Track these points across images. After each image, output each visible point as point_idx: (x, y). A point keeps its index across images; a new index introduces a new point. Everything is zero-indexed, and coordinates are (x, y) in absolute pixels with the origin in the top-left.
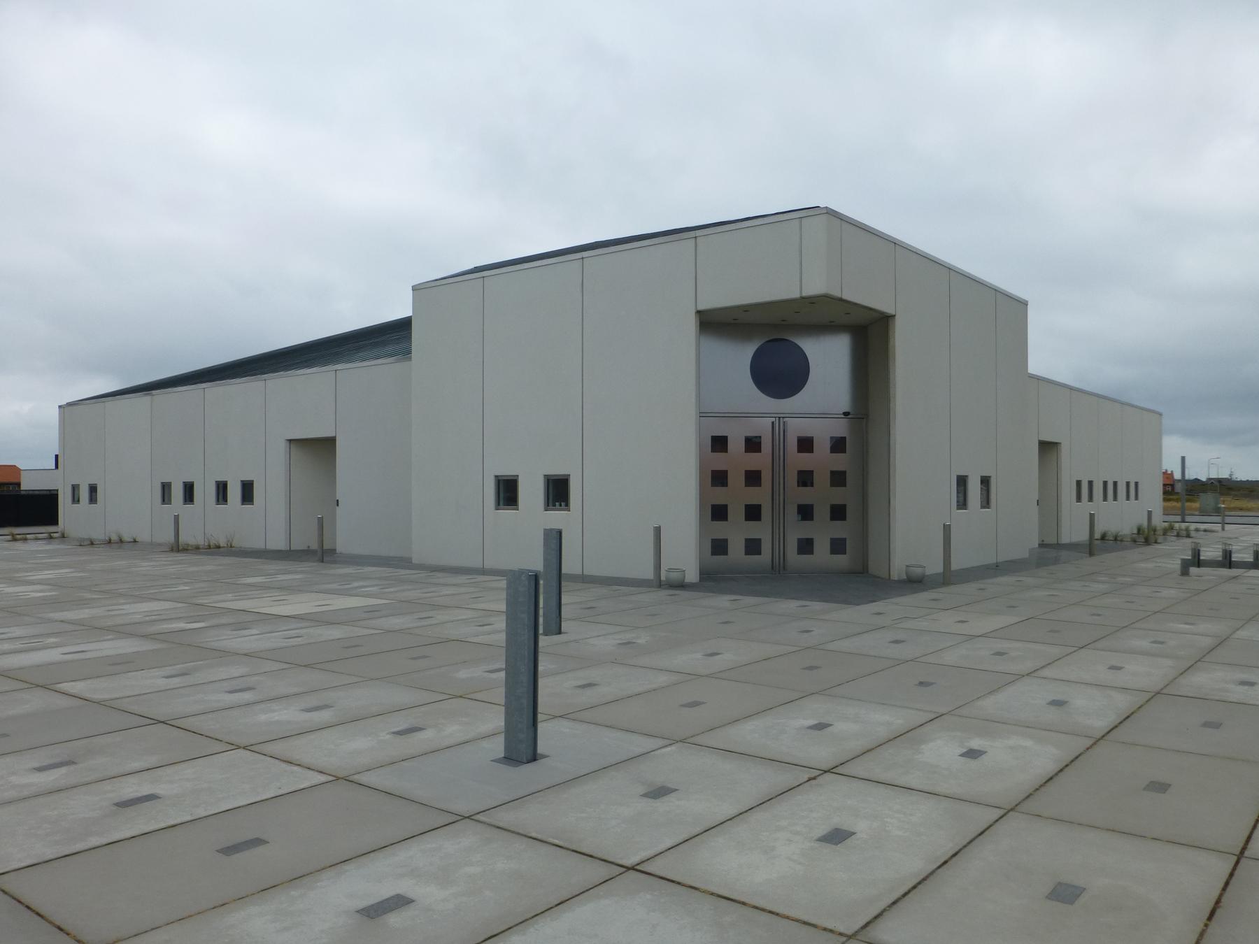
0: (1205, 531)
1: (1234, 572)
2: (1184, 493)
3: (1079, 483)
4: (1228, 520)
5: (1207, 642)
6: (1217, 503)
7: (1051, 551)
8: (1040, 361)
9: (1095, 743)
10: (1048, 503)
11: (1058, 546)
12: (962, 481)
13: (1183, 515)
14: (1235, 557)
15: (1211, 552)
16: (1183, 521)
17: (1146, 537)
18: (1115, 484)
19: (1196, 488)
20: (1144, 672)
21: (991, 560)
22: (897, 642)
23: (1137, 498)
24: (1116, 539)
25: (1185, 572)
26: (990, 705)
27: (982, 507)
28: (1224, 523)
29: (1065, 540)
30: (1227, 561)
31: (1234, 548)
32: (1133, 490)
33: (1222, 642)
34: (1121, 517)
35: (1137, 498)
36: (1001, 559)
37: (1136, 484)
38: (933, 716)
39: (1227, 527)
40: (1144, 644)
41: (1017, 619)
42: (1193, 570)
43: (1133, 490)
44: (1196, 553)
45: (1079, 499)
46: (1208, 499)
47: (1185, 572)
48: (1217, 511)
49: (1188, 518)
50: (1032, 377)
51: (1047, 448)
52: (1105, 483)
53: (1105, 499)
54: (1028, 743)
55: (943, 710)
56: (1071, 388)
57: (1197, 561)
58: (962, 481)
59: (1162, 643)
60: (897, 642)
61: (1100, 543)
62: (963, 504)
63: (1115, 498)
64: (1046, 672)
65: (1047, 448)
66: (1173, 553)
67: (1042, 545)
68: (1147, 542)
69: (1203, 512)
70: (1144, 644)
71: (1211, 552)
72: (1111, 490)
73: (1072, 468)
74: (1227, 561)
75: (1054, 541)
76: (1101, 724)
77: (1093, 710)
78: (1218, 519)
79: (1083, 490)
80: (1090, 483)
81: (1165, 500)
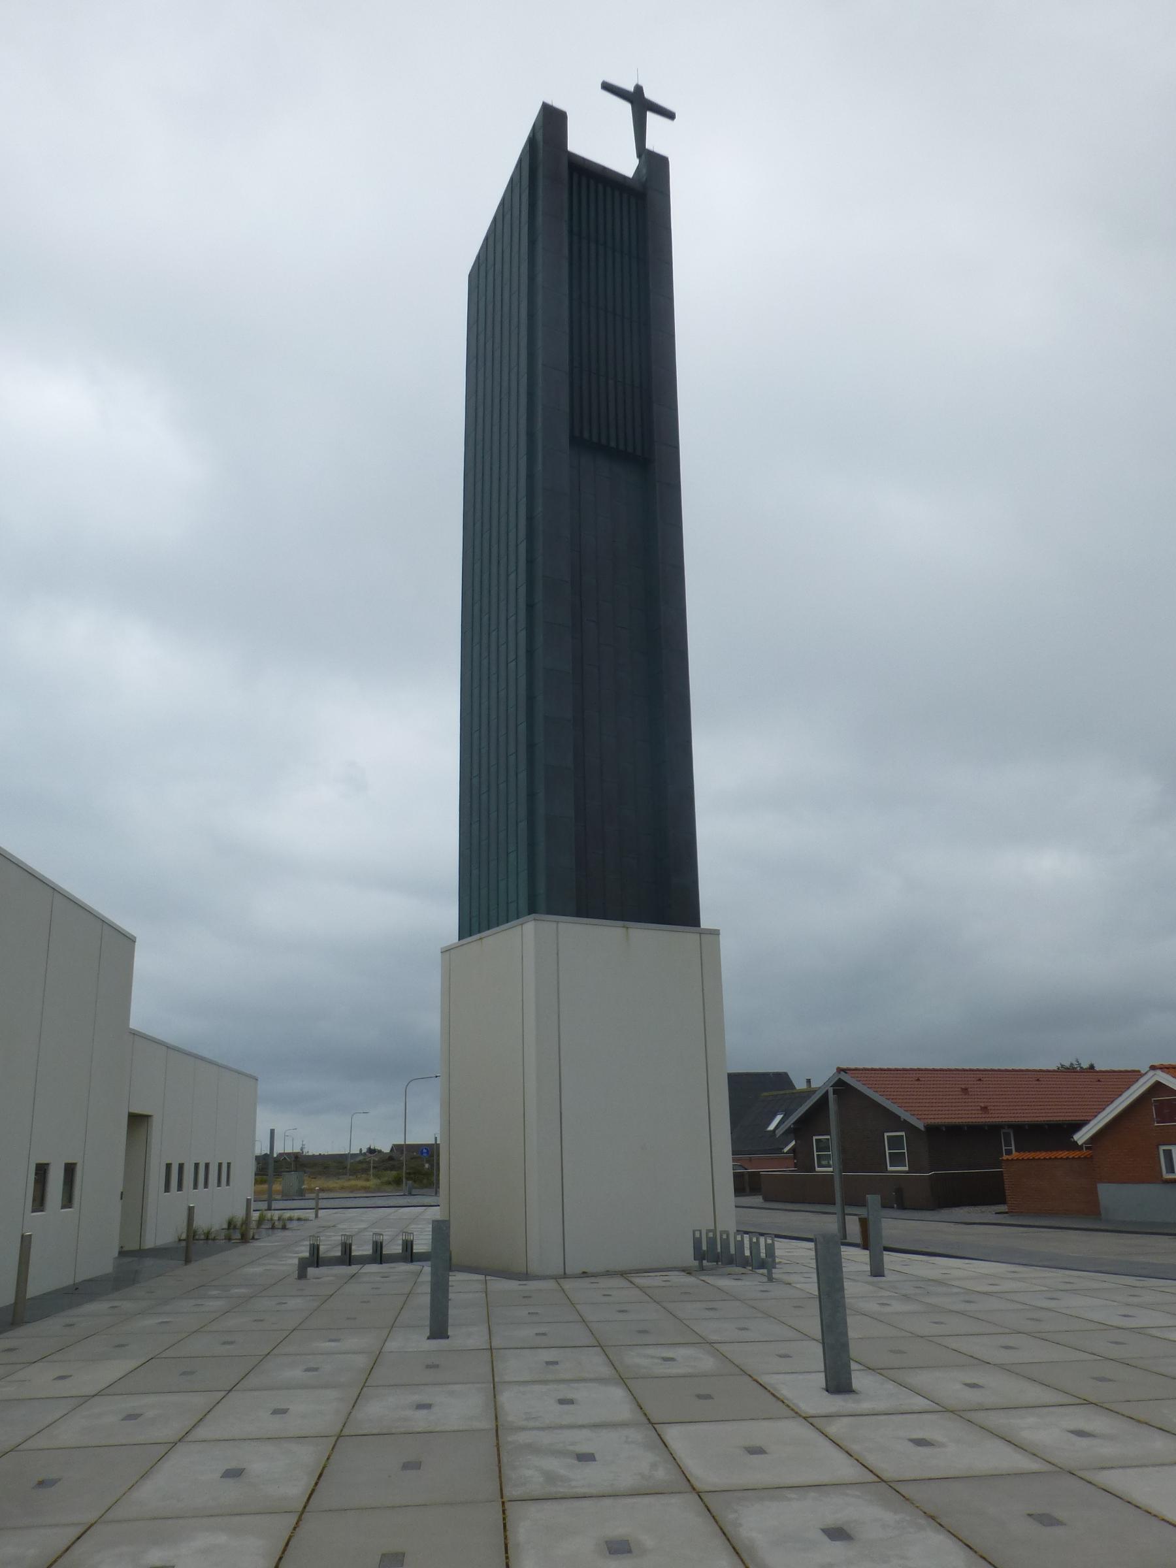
0: (299, 1219)
1: (353, 1269)
2: (281, 1171)
3: (169, 1166)
4: (322, 1204)
5: (362, 1361)
6: (302, 1182)
7: (134, 1264)
8: (144, 1013)
9: (300, 1519)
10: (133, 1199)
11: (141, 1253)
12: (42, 1171)
13: (270, 1201)
14: (356, 1252)
15: (330, 1247)
16: (269, 1209)
17: (240, 1233)
18: (181, 1166)
19: (299, 1163)
20: (316, 1411)
21: (67, 1281)
22: (1007, 1348)
23: (228, 1183)
24: (207, 1239)
25: (302, 1275)
26: (151, 1494)
27: (63, 1207)
28: (317, 1209)
29: (149, 1244)
30: (347, 1257)
31: (385, 1238)
32: (225, 1173)
33: (377, 1360)
34: (219, 1206)
35: (228, 1183)
36: (79, 1279)
37: (229, 1164)
38: (81, 1530)
39: (320, 1212)
40: (296, 1373)
41: (133, 1364)
42: (311, 1271)
43: (225, 1173)
44: (315, 1249)
45: (167, 1188)
46: (291, 1179)
47: (302, 1275)
48: (301, 1194)
49: (275, 1205)
50: (135, 1034)
51: (138, 1121)
52: (197, 1165)
53: (219, 1184)
54: (222, 1539)
55: (90, 1517)
56: (169, 1047)
57: (316, 1258)
58: (42, 1171)
59: (316, 1369)
60: (1007, 1348)
61: (193, 1245)
62: (39, 1202)
63: (206, 1185)
64: (201, 1432)
65: (138, 1121)
66: (279, 1255)
67: (122, 1253)
68: (245, 1239)
69: (286, 1196)
70: (296, 1373)
71: (330, 1247)
72: (203, 1174)
73: (165, 1146)
74: (347, 1257)
75: (135, 1247)
76: (296, 1490)
77: (282, 1473)
78: (312, 1204)
79: (174, 1177)
80: (181, 1166)
81: (256, 1182)
